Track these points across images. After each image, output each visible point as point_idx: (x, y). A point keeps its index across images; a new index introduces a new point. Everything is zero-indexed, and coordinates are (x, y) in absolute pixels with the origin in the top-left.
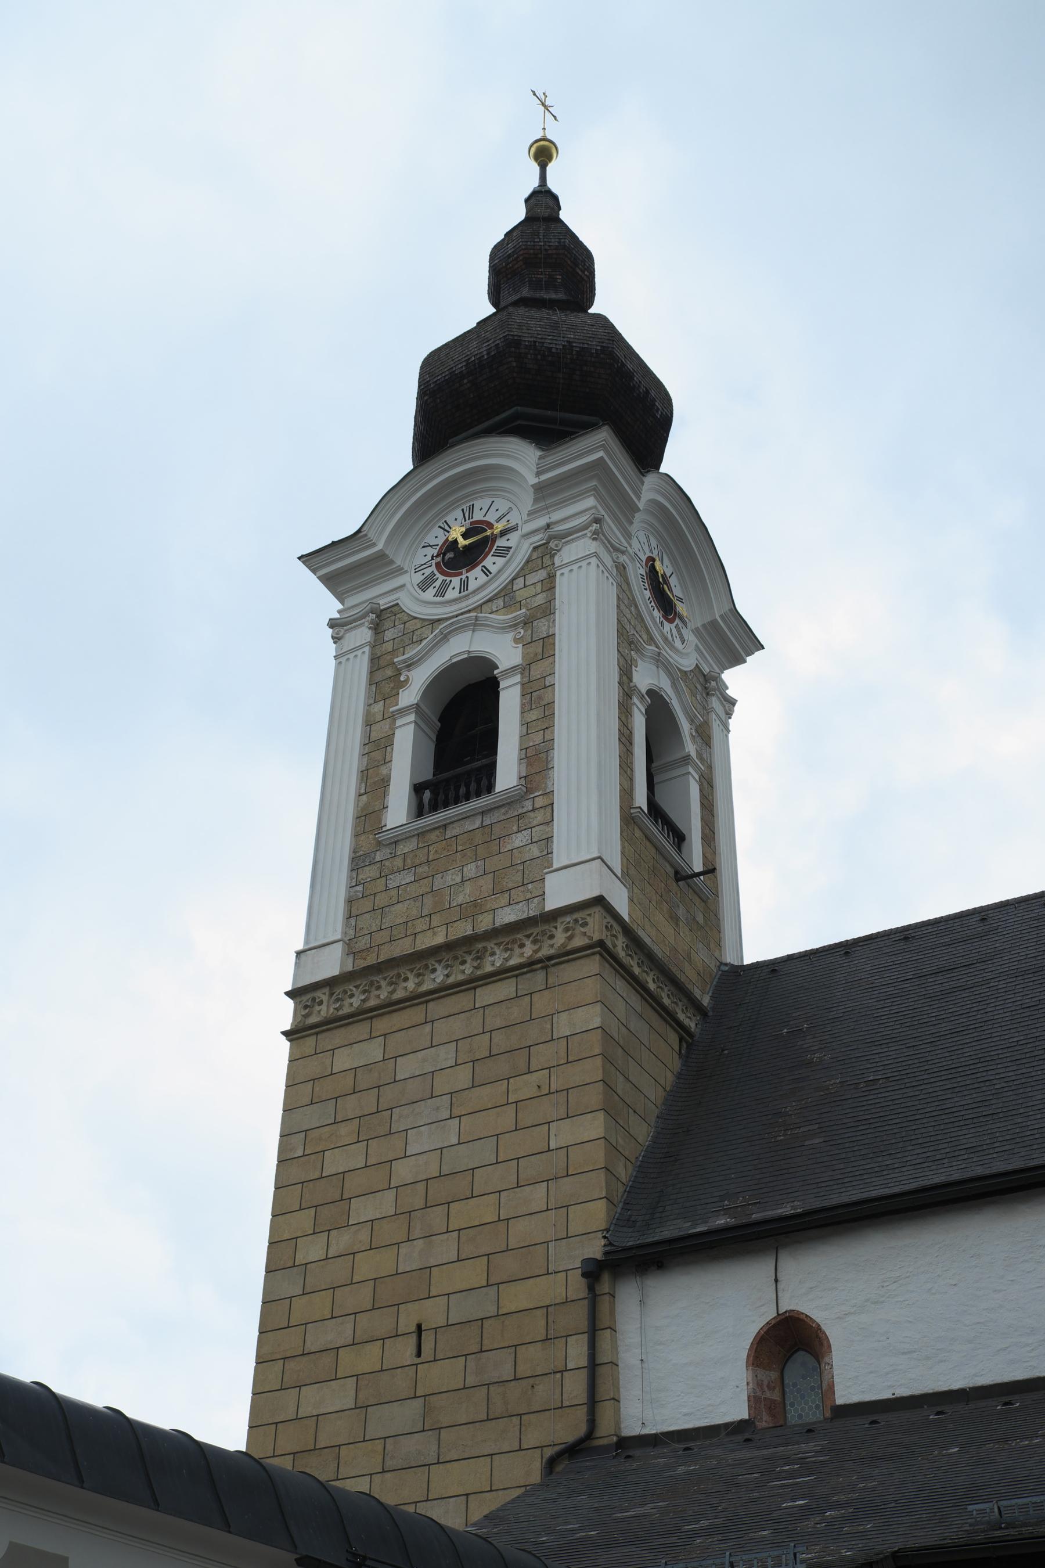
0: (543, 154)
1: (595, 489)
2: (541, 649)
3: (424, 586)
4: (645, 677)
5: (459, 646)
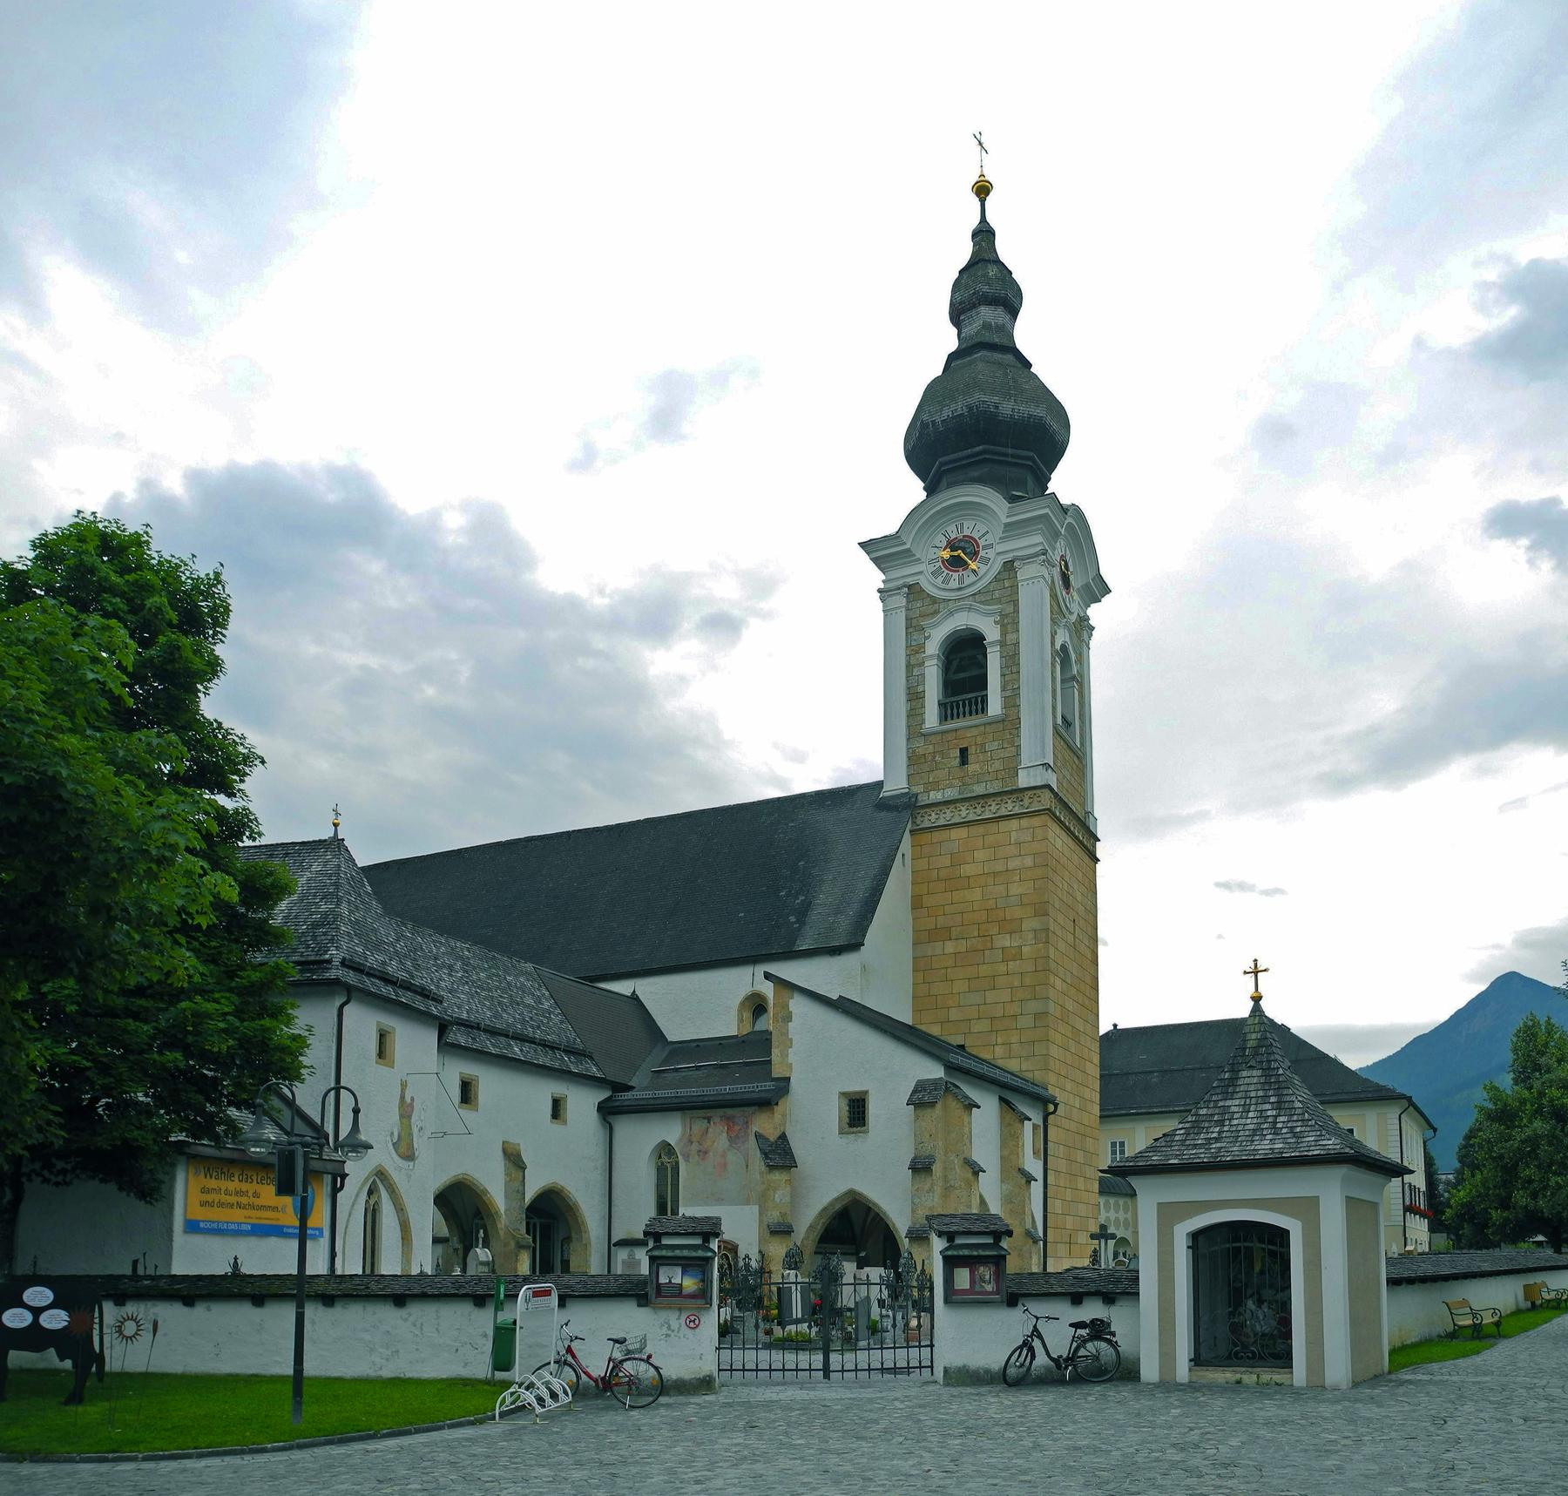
0: (982, 190)
2: (1009, 623)
4: (1062, 637)
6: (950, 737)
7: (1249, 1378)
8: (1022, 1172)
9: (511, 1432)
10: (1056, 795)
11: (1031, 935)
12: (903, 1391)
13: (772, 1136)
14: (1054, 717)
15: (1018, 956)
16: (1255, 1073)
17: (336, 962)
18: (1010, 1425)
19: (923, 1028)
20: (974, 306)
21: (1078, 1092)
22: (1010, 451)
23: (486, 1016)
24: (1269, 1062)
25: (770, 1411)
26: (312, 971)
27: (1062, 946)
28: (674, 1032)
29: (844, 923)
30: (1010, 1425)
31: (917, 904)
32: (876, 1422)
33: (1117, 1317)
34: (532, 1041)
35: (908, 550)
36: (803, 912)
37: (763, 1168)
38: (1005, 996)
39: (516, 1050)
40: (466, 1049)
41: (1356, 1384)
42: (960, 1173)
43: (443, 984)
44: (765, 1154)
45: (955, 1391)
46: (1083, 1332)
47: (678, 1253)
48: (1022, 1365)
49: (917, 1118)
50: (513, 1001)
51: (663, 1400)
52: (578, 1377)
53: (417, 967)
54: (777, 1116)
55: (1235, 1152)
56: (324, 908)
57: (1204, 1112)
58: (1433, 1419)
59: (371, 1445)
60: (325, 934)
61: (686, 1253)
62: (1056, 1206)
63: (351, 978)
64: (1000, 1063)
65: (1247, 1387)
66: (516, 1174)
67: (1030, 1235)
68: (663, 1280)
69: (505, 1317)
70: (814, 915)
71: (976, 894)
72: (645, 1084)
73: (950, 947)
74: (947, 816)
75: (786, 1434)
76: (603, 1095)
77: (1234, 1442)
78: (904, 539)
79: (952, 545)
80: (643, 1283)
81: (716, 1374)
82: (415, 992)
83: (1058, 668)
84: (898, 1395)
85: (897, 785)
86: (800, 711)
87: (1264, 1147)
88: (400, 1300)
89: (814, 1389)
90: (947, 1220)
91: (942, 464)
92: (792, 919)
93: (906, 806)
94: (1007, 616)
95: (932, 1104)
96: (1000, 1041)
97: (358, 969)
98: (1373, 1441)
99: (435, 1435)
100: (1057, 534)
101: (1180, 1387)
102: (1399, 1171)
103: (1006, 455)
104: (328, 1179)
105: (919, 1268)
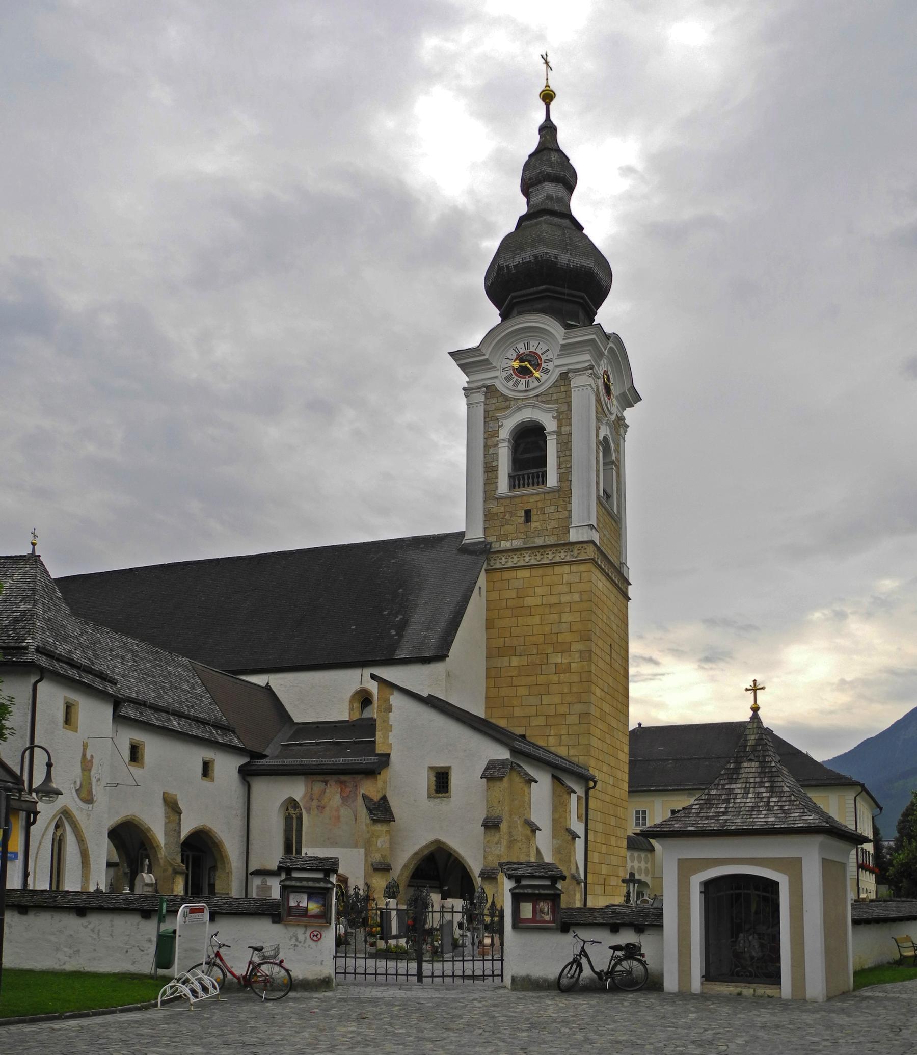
0: (548, 97)
2: (564, 418)
3: (508, 378)
4: (604, 431)
5: (526, 415)
6: (517, 501)
7: (748, 991)
8: (569, 831)
9: (171, 1017)
10: (598, 548)
11: (577, 655)
12: (479, 993)
13: (376, 797)
14: (598, 490)
15: (568, 670)
16: (753, 764)
17: (32, 649)
18: (565, 1022)
19: (493, 721)
21: (612, 771)
22: (566, 291)
23: (151, 697)
24: (764, 756)
25: (376, 1006)
26: (13, 655)
27: (601, 664)
28: (299, 716)
29: (434, 639)
30: (565, 1022)
31: (490, 625)
32: (460, 1017)
33: (646, 943)
34: (187, 717)
35: (487, 360)
36: (402, 627)
37: (368, 821)
38: (557, 699)
39: (175, 723)
40: (135, 721)
41: (829, 999)
42: (521, 831)
43: (117, 670)
44: (370, 811)
45: (521, 994)
46: (620, 953)
47: (305, 884)
48: (572, 977)
49: (488, 788)
50: (173, 687)
51: (292, 994)
52: (225, 975)
53: (96, 656)
54: (380, 783)
55: (738, 823)
56: (23, 607)
57: (714, 792)
58: (891, 1027)
59: (56, 1025)
60: (24, 627)
61: (311, 884)
62: (594, 857)
63: (44, 661)
64: (553, 749)
65: (746, 998)
66: (174, 817)
67: (575, 878)
68: (293, 903)
69: (166, 927)
70: (410, 631)
71: (536, 620)
72: (276, 753)
73: (515, 661)
74: (514, 560)
75: (390, 1024)
76: (243, 761)
77: (740, 1041)
78: (484, 351)
80: (276, 905)
81: (333, 976)
82: (96, 675)
83: (601, 454)
84: (476, 996)
85: (476, 534)
86: (414, 473)
87: (761, 819)
88: (81, 911)
89: (410, 989)
90: (515, 866)
91: (513, 298)
92: (393, 632)
93: (481, 551)
95: (501, 779)
96: (552, 733)
97: (50, 655)
98: (847, 1042)
99: (108, 1017)
100: (600, 355)
101: (694, 997)
102: (857, 839)
103: (563, 294)
104: (23, 815)
105: (490, 900)
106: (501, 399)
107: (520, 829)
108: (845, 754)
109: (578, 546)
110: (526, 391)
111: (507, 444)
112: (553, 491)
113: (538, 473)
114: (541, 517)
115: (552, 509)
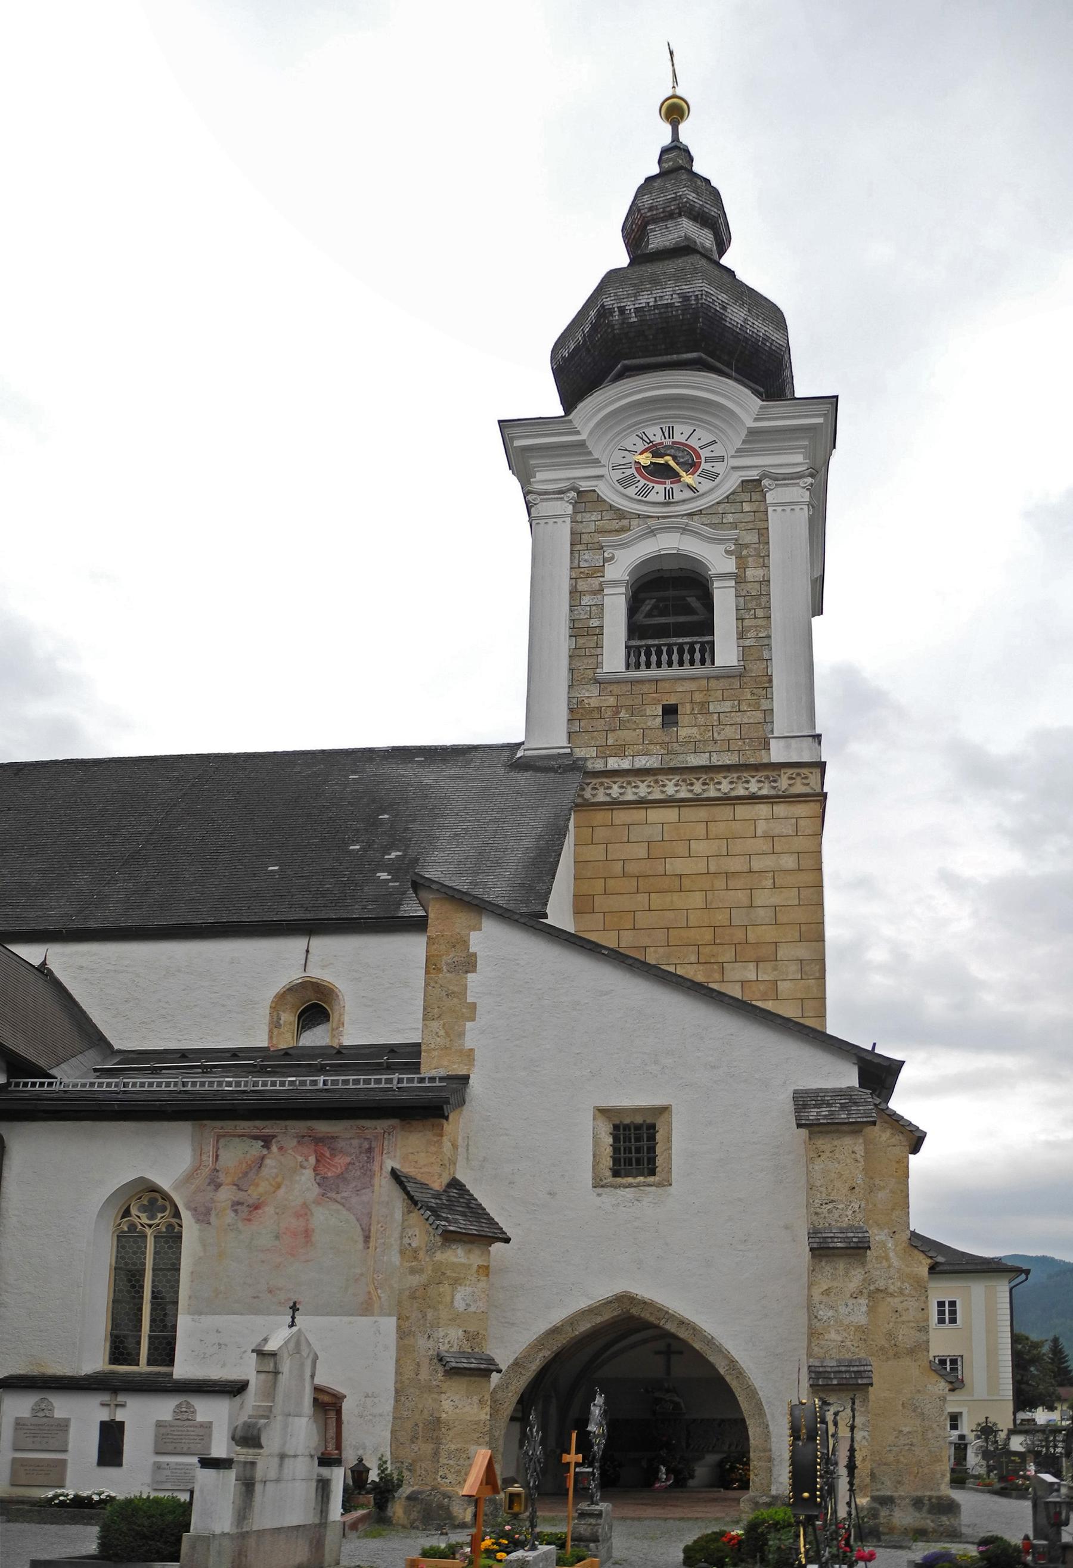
0: (675, 112)
1: (805, 447)
6: (645, 688)
11: (793, 969)
20: (671, 216)
35: (582, 444)
71: (697, 899)
79: (656, 451)
85: (555, 739)
86: (408, 625)
94: (747, 546)
106: (607, 515)
107: (895, 1262)
108: (955, 1250)
109: (790, 771)
110: (667, 504)
111: (623, 590)
112: (727, 674)
113: (692, 645)
114: (701, 720)
115: (727, 706)
